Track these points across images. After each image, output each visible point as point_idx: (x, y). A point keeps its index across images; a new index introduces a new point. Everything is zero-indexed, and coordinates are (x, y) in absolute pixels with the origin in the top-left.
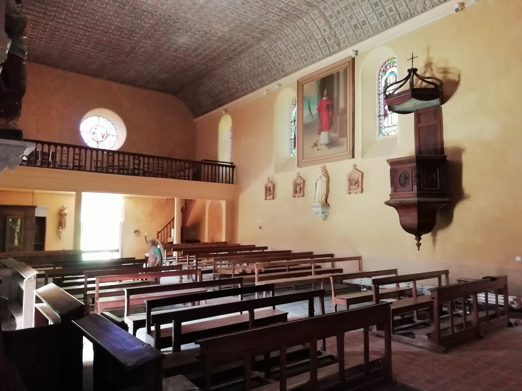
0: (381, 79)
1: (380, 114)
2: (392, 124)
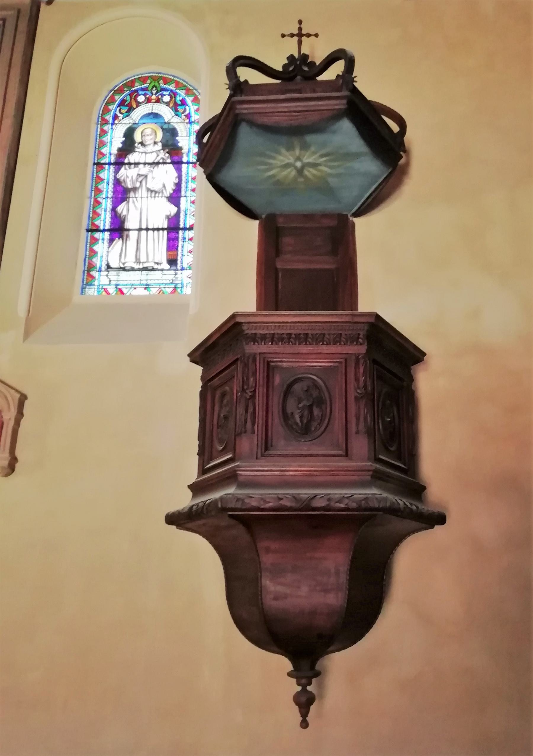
0: (111, 122)
1: (97, 223)
2: (138, 261)
